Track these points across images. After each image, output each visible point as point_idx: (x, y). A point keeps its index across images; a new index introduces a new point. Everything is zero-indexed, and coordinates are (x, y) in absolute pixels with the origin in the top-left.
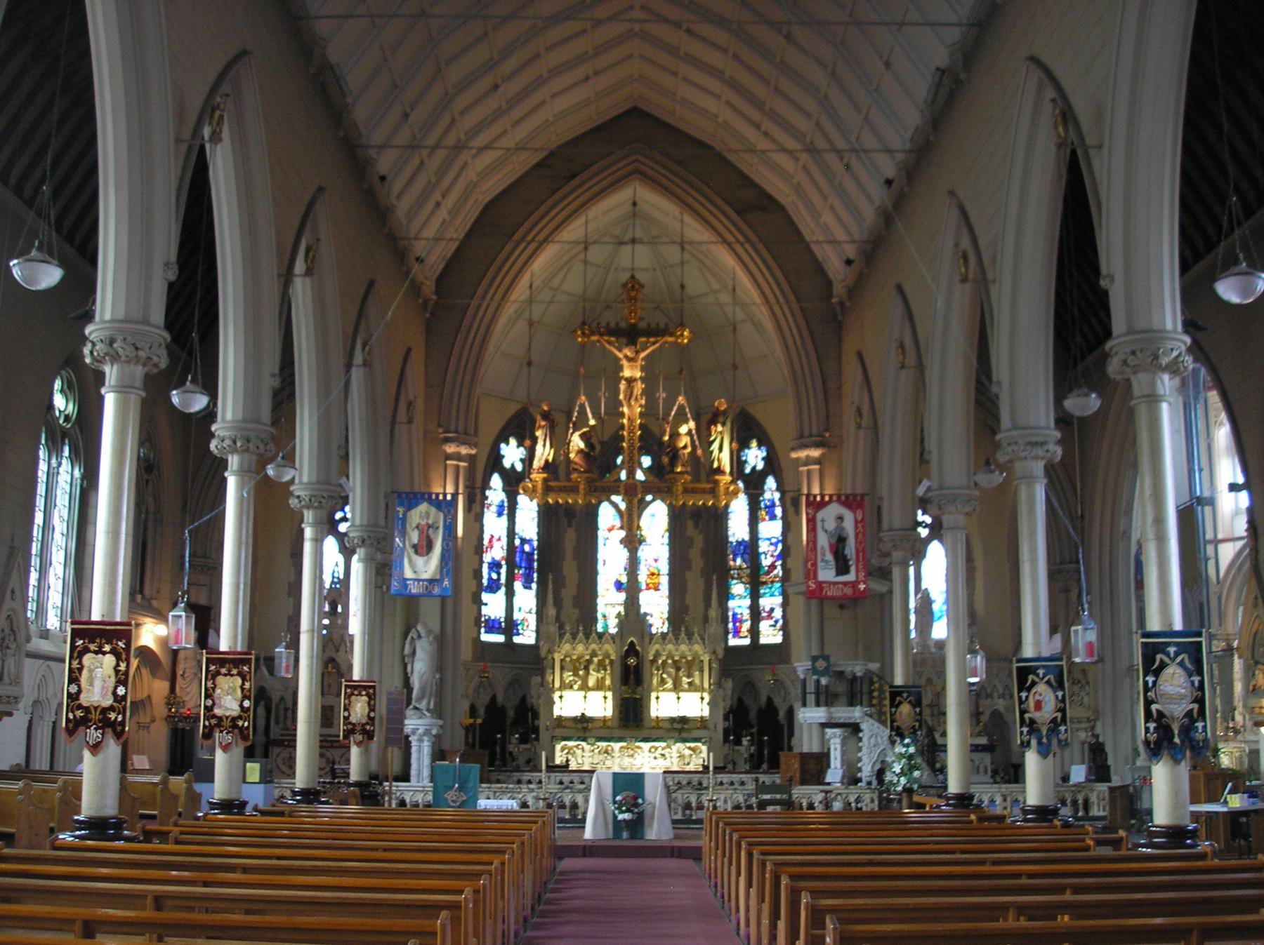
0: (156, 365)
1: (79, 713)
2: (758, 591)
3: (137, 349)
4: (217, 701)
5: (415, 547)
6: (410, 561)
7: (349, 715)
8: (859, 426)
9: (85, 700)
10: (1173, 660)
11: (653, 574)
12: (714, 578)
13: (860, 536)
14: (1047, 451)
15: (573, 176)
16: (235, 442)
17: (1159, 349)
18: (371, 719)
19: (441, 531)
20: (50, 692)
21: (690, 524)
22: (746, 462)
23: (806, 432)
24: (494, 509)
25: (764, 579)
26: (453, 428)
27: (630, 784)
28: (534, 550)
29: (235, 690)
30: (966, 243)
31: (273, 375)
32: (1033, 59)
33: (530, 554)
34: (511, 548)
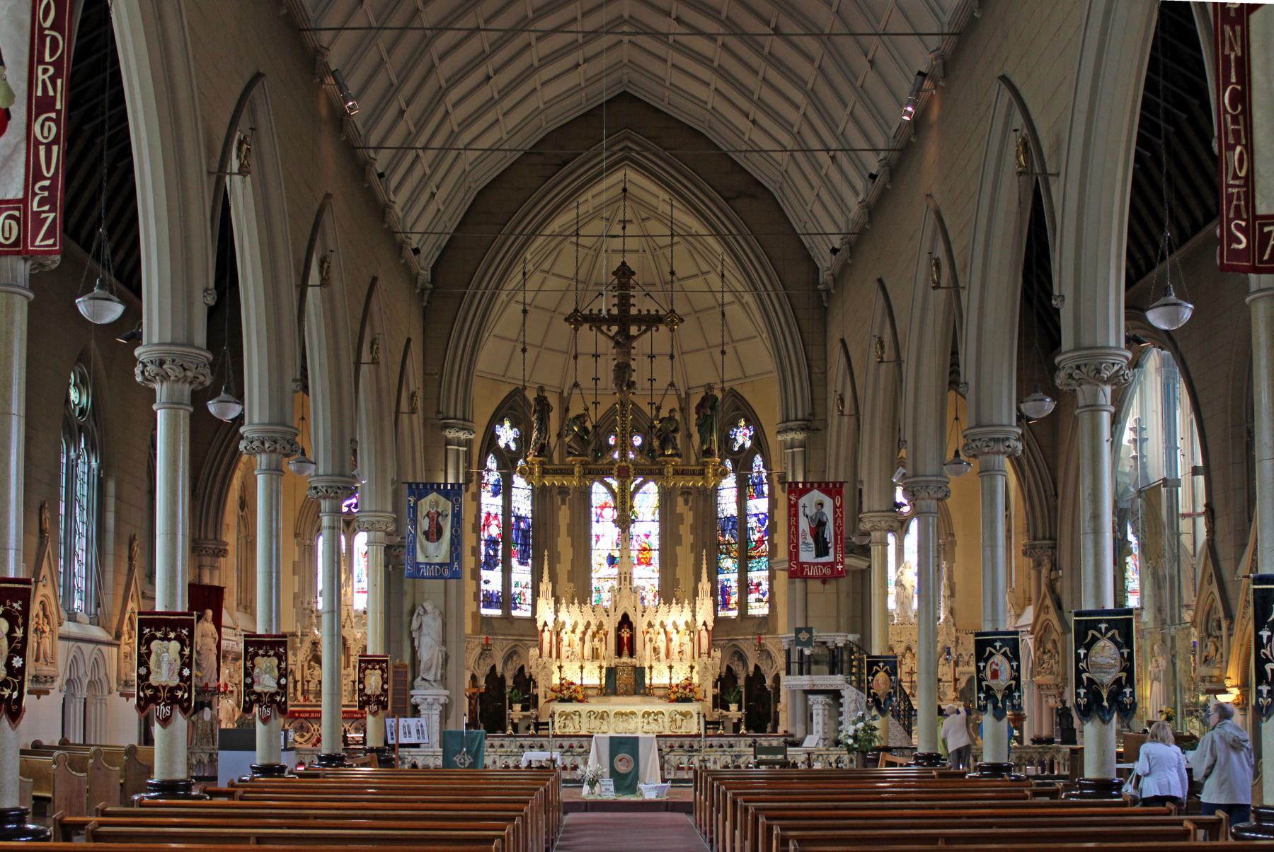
0: (201, 383)
1: (365, 698)
2: (747, 566)
3: (185, 369)
4: (256, 679)
5: (425, 533)
6: (422, 547)
7: (364, 688)
8: (842, 414)
9: (368, 691)
10: (1105, 635)
11: (645, 549)
12: (704, 553)
13: (839, 521)
14: (1009, 446)
15: (565, 163)
16: (263, 443)
17: (1101, 363)
18: (385, 691)
19: (450, 518)
20: (81, 671)
21: (680, 500)
22: (735, 440)
23: (792, 416)
24: (490, 488)
25: (754, 553)
26: (452, 414)
27: (624, 746)
28: (529, 527)
29: (272, 670)
30: (940, 252)
31: (295, 380)
32: (1005, 79)
33: (525, 532)
34: (506, 526)
